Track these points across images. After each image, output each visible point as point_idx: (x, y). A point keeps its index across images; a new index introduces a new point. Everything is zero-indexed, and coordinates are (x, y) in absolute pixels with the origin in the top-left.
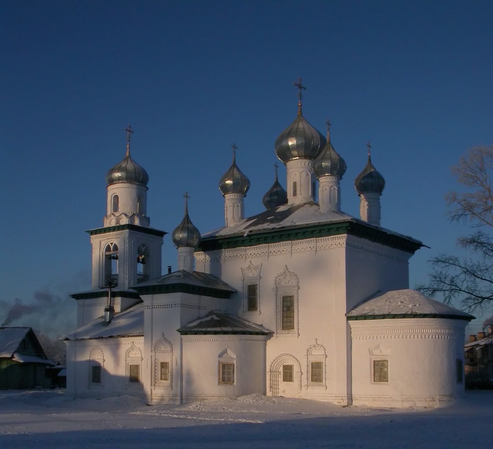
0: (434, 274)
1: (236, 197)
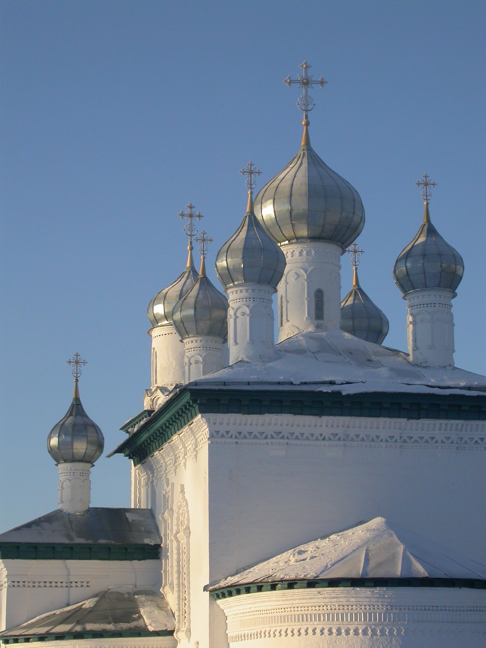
1: (199, 344)
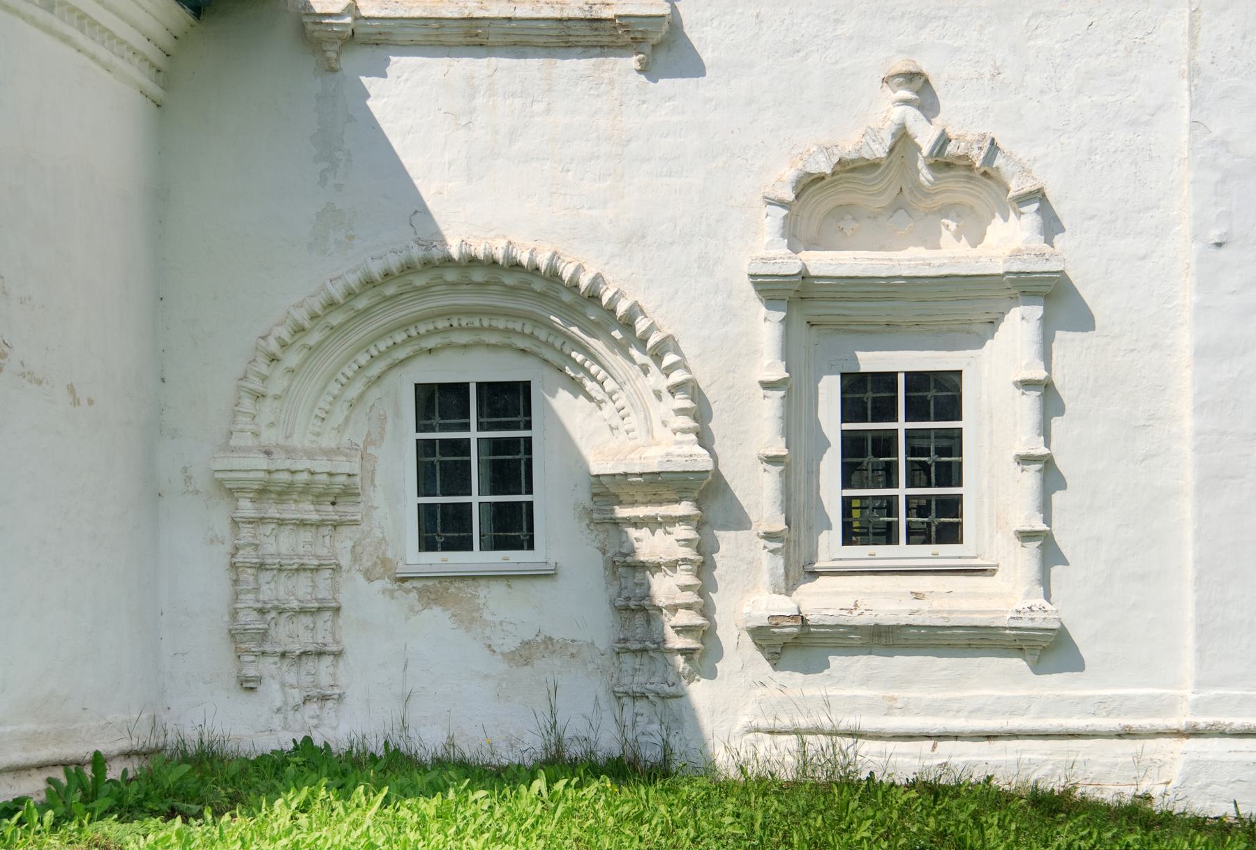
0: (390, 742)
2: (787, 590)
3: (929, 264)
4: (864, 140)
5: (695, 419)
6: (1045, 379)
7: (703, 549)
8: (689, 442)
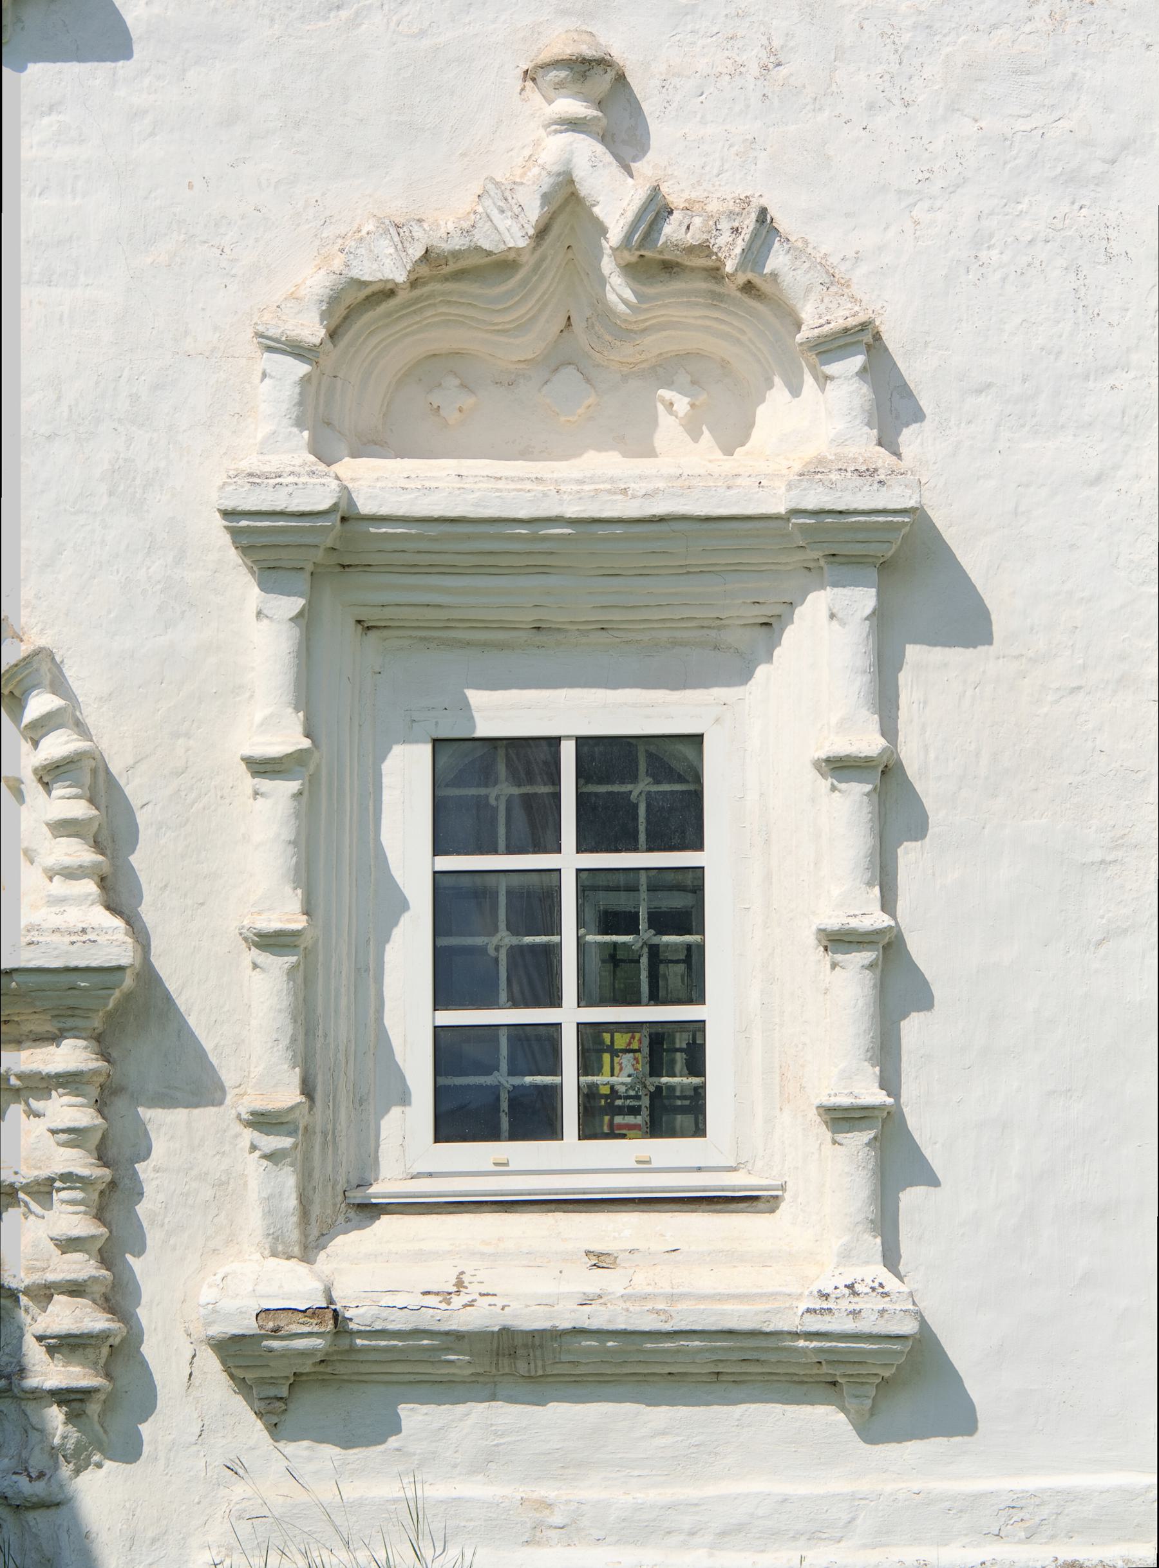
2: (305, 1247)
3: (625, 491)
4: (480, 209)
5: (97, 845)
6: (881, 755)
7: (112, 1153)
8: (79, 900)
